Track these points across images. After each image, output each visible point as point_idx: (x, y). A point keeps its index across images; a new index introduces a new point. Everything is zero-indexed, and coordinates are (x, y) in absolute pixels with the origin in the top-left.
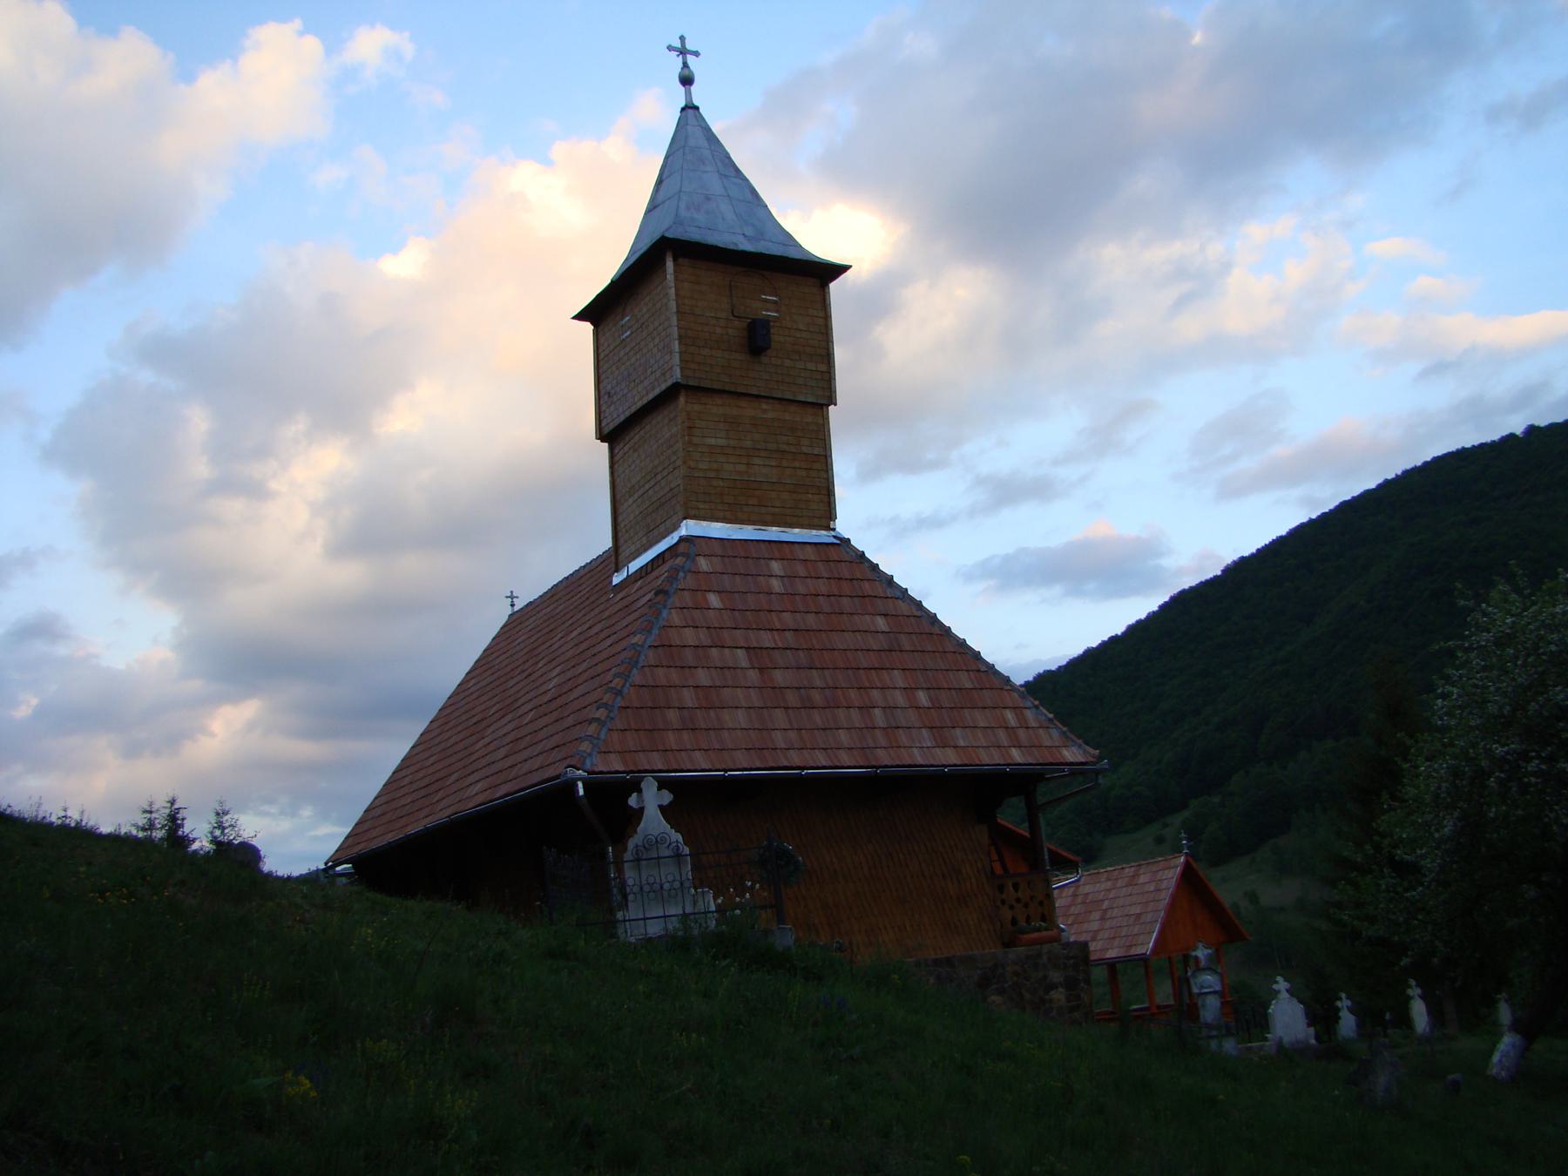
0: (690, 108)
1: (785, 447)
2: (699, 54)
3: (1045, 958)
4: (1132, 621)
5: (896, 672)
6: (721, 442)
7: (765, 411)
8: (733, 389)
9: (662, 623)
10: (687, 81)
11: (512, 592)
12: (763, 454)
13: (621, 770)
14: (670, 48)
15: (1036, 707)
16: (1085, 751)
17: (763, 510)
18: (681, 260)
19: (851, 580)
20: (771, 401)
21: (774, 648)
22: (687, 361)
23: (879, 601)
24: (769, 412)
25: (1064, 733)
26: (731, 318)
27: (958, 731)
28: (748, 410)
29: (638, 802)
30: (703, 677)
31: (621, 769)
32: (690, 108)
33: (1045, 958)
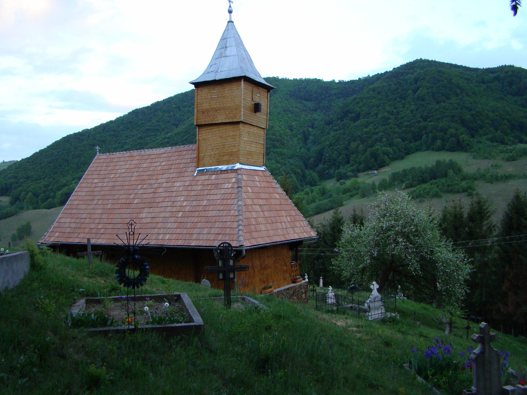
0: (230, 22)
1: (257, 141)
4: (118, 116)
6: (247, 139)
9: (243, 198)
10: (230, 12)
12: (254, 143)
18: (245, 82)
30: (254, 215)
32: (230, 22)
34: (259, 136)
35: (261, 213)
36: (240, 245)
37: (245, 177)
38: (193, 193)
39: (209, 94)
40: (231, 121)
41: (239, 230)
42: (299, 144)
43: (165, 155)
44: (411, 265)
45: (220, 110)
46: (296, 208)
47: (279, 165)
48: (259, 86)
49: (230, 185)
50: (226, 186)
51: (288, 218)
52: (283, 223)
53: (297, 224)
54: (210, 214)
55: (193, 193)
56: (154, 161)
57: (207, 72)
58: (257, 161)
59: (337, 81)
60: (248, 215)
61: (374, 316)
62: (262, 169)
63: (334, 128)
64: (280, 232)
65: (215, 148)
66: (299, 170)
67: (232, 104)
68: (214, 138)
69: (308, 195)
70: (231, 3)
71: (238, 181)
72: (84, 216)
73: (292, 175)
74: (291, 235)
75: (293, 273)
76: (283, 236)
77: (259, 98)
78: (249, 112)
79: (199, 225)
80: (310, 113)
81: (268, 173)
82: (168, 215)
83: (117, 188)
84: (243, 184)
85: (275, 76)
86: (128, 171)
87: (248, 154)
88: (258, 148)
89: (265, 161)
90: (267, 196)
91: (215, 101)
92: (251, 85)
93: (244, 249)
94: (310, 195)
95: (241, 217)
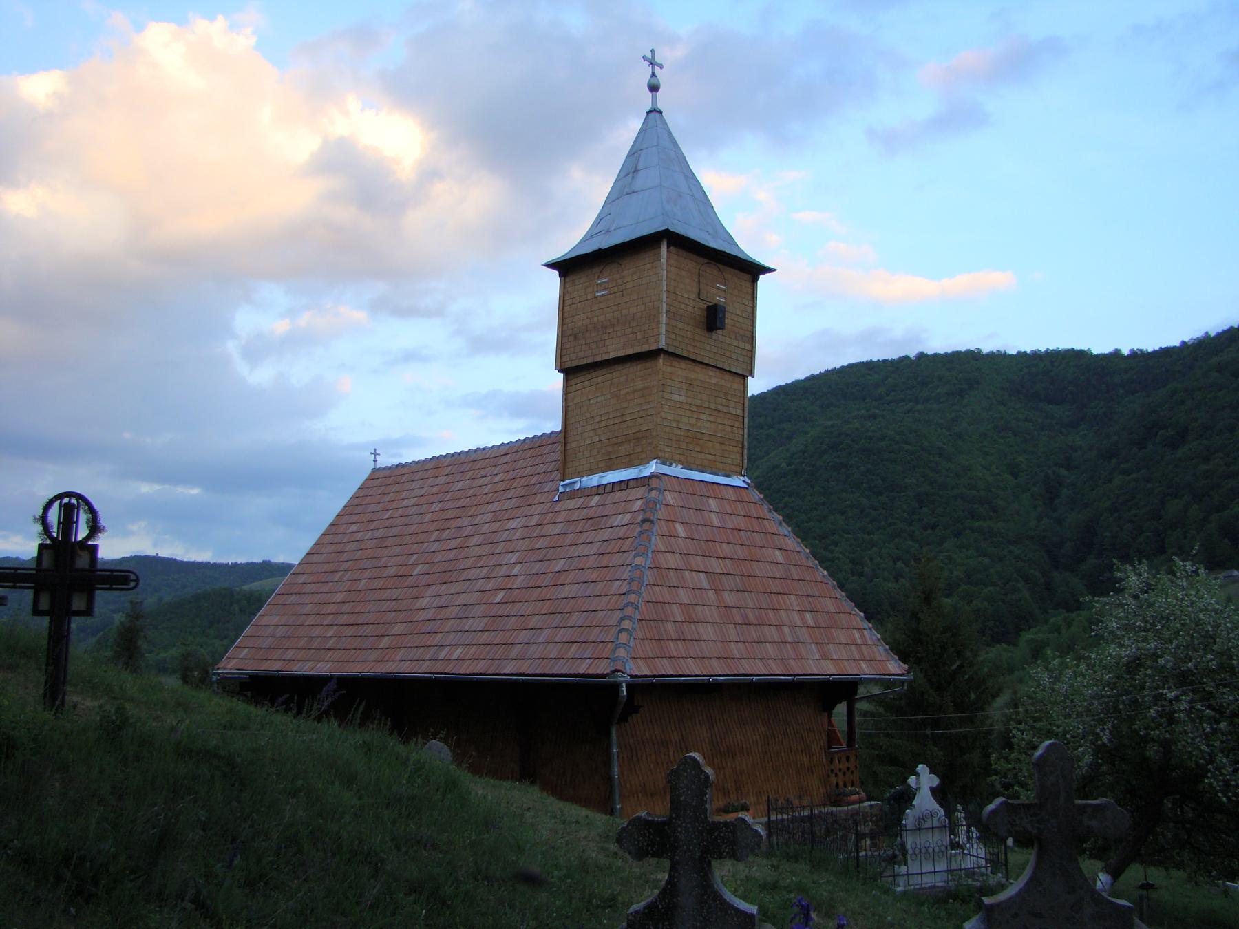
0: (654, 111)
1: (720, 407)
2: (643, 57)
5: (792, 596)
6: (683, 399)
7: (710, 377)
9: (653, 548)
10: (654, 88)
11: (375, 450)
12: (707, 411)
13: (648, 674)
14: (644, 58)
15: (870, 629)
16: (899, 665)
17: (703, 455)
19: (758, 518)
20: (715, 369)
21: (721, 574)
22: (669, 332)
23: (775, 537)
24: (713, 378)
25: (887, 650)
26: (698, 300)
27: (831, 647)
28: (699, 374)
29: (916, 784)
30: (683, 595)
31: (649, 673)
32: (654, 111)
34: (726, 394)
35: (711, 594)
36: (613, 669)
37: (670, 498)
38: (540, 543)
39: (590, 290)
40: (637, 350)
41: (621, 631)
42: (1035, 507)
43: (506, 459)
44: (1212, 772)
45: (613, 326)
46: (839, 594)
47: (986, 561)
48: (720, 263)
49: (628, 516)
50: (617, 520)
51: (808, 616)
52: (786, 629)
53: (841, 636)
54: (566, 591)
55: (540, 543)
56: (482, 473)
57: (589, 236)
58: (718, 459)
59: (1126, 352)
60: (662, 594)
61: (916, 880)
62: (738, 481)
63: (1122, 466)
64: (771, 650)
65: (601, 425)
66: (1037, 573)
67: (641, 308)
68: (599, 399)
69: (1060, 633)
70: (657, 69)
71: (650, 505)
72: (308, 609)
73: (1020, 585)
74: (811, 661)
75: (833, 777)
76: (779, 662)
77: (722, 294)
78: (688, 328)
79: (534, 622)
80: (1061, 433)
81: (756, 495)
82: (473, 598)
83: (390, 541)
84: (661, 513)
85: (972, 348)
86: (424, 500)
87: (688, 440)
88: (720, 427)
89: (745, 462)
90: (740, 552)
91: (601, 306)
92: (694, 257)
93: (623, 680)
94: (1064, 631)
95: (632, 598)
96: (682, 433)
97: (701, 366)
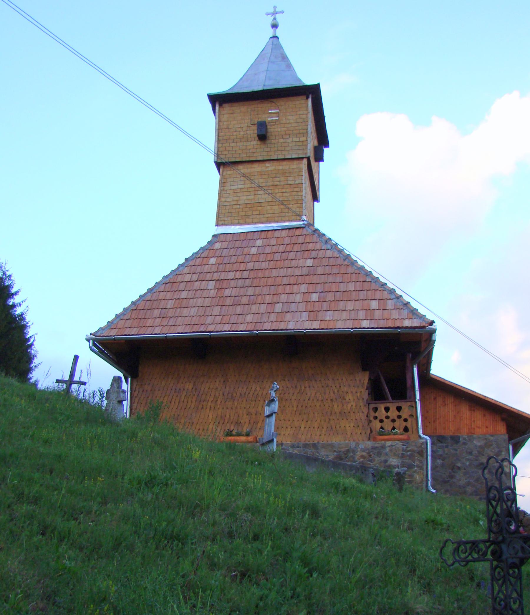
0: (275, 37)
2: (266, 14)
3: (388, 450)
8: (248, 159)
10: (275, 26)
17: (262, 216)
24: (269, 167)
33: (388, 450)
77: (275, 115)
78: (254, 143)
96: (241, 207)
97: (268, 162)
